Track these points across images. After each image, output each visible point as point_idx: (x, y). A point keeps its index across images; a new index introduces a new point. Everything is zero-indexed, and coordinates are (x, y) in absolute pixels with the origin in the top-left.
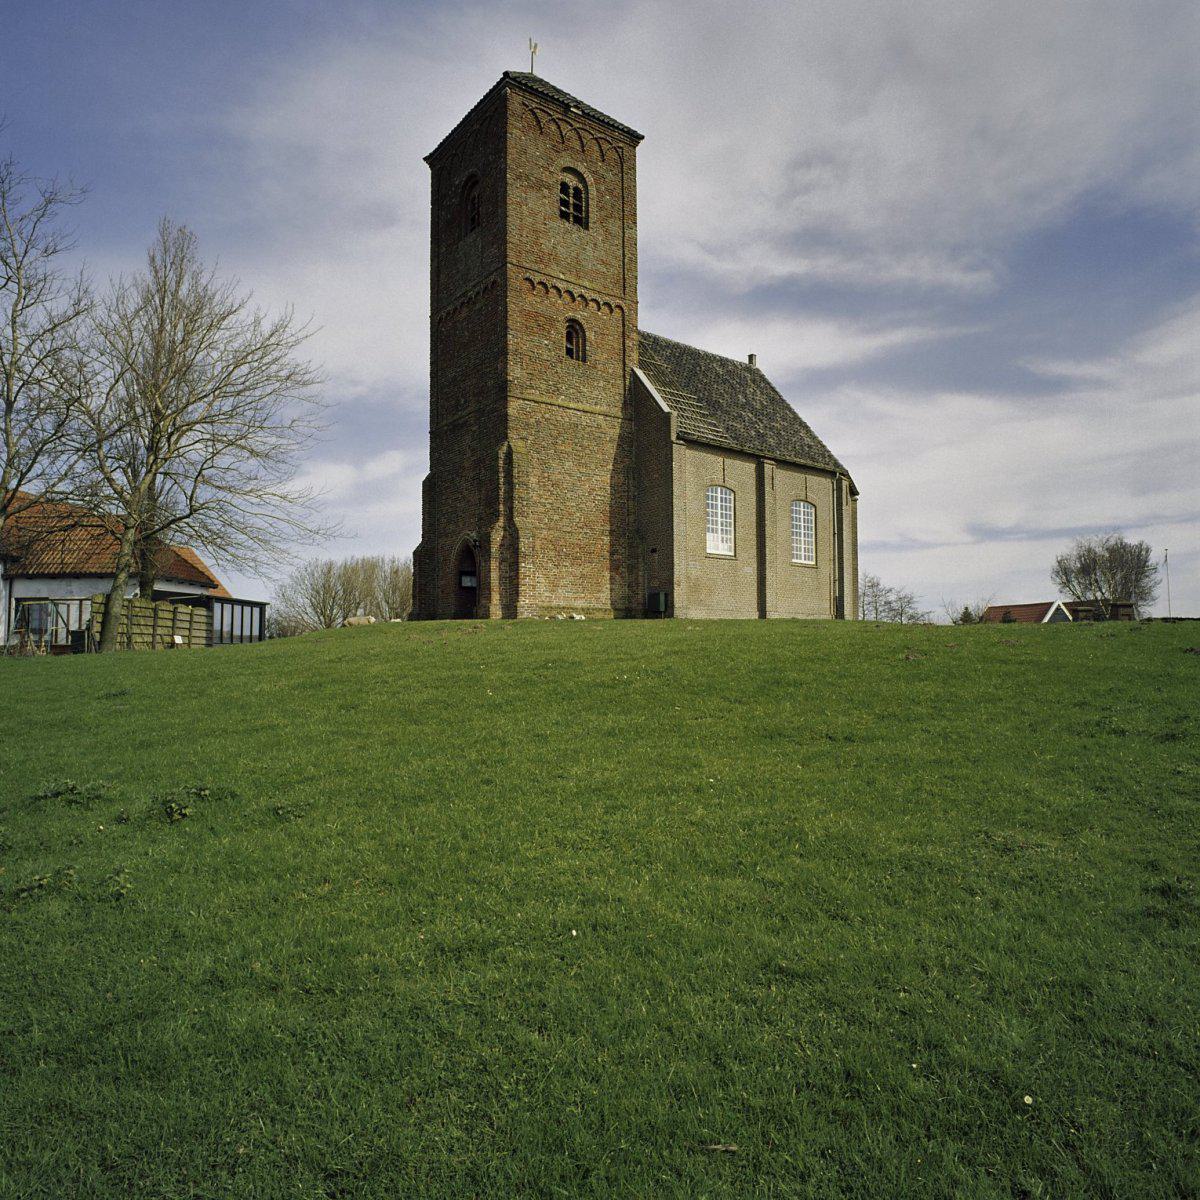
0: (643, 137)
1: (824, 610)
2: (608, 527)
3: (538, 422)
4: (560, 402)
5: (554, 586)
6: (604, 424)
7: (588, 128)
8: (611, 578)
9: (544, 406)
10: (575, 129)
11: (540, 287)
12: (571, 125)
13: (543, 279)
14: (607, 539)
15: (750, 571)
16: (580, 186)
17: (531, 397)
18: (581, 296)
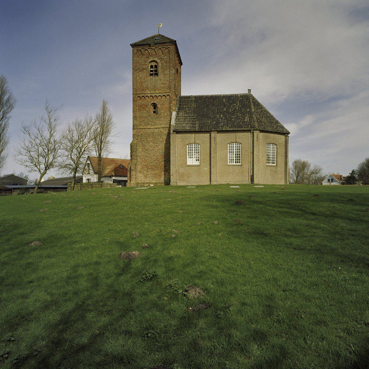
0: (130, 45)
1: (247, 181)
2: (163, 160)
3: (141, 134)
4: (149, 127)
5: (146, 177)
6: (163, 130)
7: (157, 47)
8: (165, 174)
9: (143, 129)
10: (160, 49)
11: (159, 97)
12: (152, 48)
13: (143, 95)
14: (163, 163)
15: (207, 169)
16: (157, 64)
17: (140, 128)
18: (155, 96)
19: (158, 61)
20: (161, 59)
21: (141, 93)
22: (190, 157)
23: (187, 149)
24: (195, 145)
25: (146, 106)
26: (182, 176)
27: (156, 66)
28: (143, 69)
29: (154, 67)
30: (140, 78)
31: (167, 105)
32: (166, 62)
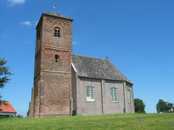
0: (43, 13)
5: (50, 110)
19: (61, 28)
20: (63, 28)
21: (48, 46)
22: (88, 96)
23: (94, 90)
24: (91, 88)
25: (51, 56)
26: (83, 110)
27: (59, 31)
28: (50, 31)
29: (57, 31)
30: (48, 36)
31: (66, 58)
32: (66, 30)
